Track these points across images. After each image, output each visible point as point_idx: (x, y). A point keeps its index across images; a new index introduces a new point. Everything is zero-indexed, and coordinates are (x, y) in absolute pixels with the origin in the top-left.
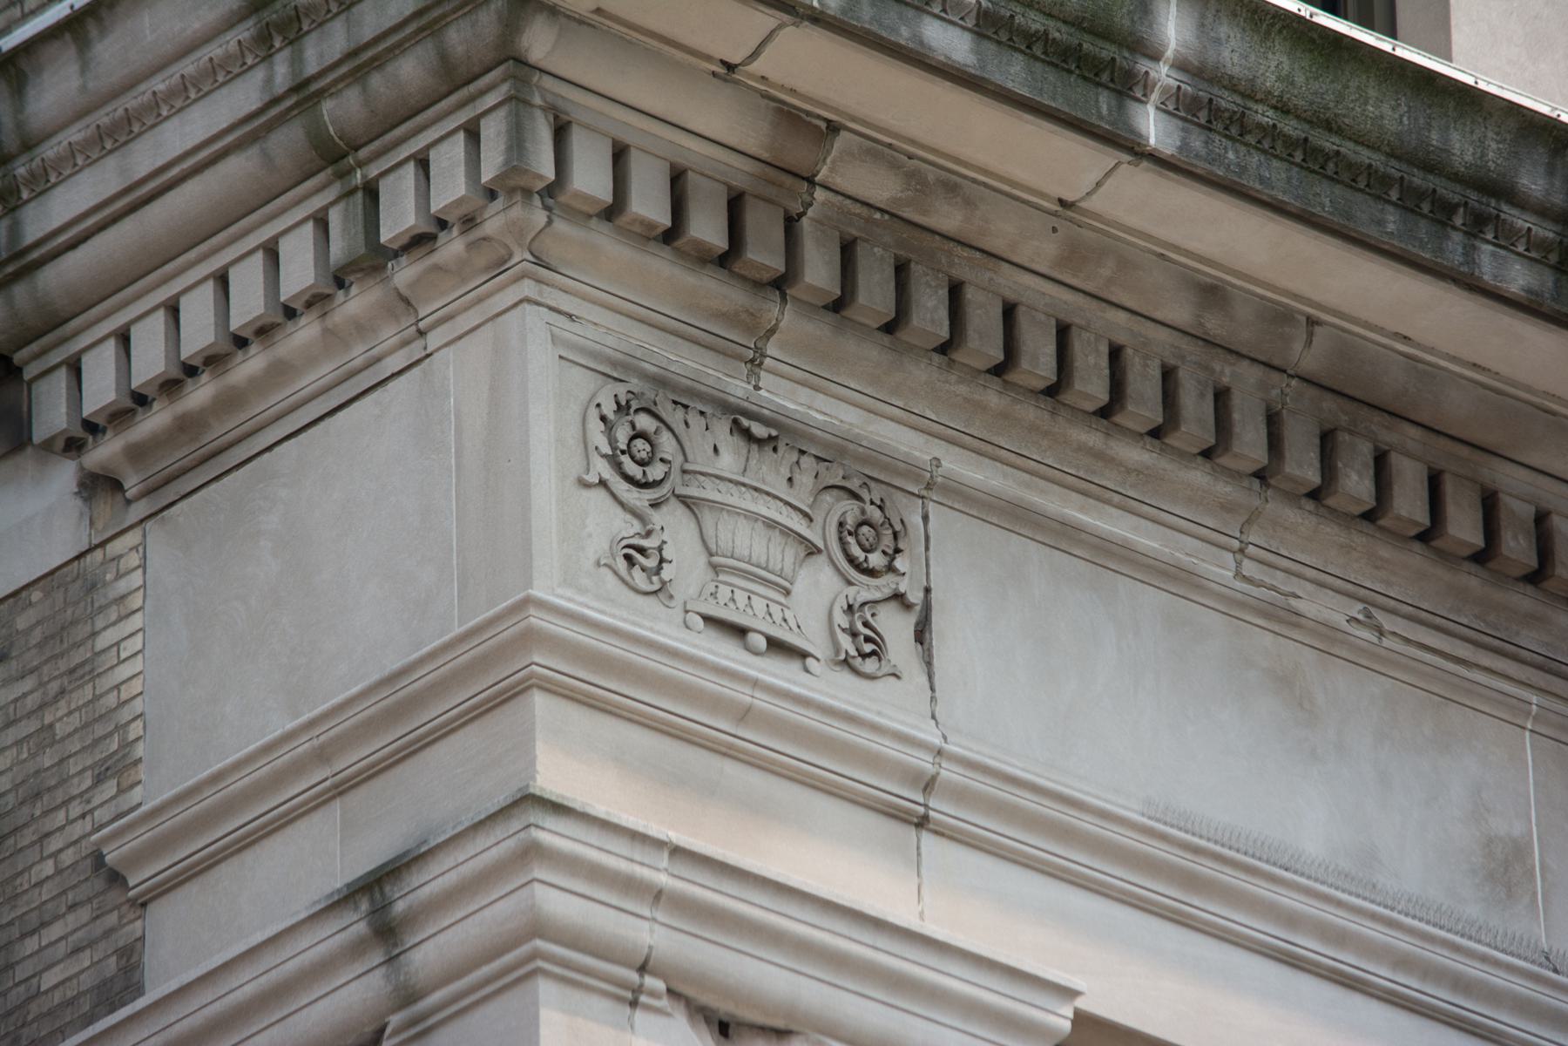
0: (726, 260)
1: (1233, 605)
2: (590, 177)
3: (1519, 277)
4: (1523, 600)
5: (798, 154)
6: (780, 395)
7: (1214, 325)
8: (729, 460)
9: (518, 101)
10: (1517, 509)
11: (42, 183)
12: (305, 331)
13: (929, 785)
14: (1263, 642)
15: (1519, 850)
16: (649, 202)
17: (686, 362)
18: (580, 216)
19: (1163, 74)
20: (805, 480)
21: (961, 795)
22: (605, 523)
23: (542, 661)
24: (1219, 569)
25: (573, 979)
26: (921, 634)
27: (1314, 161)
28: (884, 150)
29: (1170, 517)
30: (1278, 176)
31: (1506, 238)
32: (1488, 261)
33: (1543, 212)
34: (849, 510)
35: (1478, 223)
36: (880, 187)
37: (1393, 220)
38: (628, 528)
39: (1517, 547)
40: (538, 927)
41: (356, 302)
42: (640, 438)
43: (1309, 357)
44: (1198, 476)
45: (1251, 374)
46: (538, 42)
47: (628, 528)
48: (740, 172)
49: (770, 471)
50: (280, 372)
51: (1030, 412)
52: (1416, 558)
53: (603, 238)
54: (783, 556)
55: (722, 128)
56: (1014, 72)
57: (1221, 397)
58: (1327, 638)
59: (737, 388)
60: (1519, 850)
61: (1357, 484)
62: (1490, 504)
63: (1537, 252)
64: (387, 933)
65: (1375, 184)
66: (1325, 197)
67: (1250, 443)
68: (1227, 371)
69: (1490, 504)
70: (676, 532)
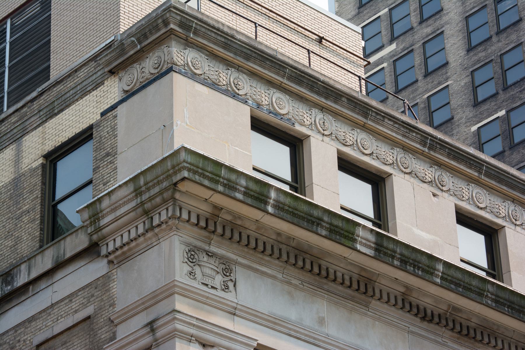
1: (282, 281)
3: (324, 233)
4: (325, 281)
5: (216, 213)
6: (213, 249)
7: (279, 239)
8: (205, 259)
9: (174, 204)
11: (103, 217)
12: (142, 239)
13: (235, 309)
14: (286, 287)
17: (199, 244)
19: (271, 201)
20: (217, 262)
21: (241, 310)
22: (187, 268)
23: (177, 289)
24: (280, 276)
25: (181, 338)
26: (235, 285)
27: (294, 215)
28: (230, 212)
30: (288, 217)
31: (322, 227)
32: (319, 230)
33: (327, 223)
35: (318, 224)
36: (229, 218)
37: (305, 224)
38: (190, 269)
40: (176, 330)
42: (192, 255)
44: (277, 262)
45: (285, 246)
46: (177, 196)
47: (190, 269)
50: (138, 245)
52: (309, 274)
53: (187, 225)
54: (213, 273)
55: (205, 209)
56: (249, 201)
58: (296, 287)
59: (207, 248)
60: (323, 318)
63: (327, 229)
65: (303, 218)
66: (296, 220)
68: (281, 246)
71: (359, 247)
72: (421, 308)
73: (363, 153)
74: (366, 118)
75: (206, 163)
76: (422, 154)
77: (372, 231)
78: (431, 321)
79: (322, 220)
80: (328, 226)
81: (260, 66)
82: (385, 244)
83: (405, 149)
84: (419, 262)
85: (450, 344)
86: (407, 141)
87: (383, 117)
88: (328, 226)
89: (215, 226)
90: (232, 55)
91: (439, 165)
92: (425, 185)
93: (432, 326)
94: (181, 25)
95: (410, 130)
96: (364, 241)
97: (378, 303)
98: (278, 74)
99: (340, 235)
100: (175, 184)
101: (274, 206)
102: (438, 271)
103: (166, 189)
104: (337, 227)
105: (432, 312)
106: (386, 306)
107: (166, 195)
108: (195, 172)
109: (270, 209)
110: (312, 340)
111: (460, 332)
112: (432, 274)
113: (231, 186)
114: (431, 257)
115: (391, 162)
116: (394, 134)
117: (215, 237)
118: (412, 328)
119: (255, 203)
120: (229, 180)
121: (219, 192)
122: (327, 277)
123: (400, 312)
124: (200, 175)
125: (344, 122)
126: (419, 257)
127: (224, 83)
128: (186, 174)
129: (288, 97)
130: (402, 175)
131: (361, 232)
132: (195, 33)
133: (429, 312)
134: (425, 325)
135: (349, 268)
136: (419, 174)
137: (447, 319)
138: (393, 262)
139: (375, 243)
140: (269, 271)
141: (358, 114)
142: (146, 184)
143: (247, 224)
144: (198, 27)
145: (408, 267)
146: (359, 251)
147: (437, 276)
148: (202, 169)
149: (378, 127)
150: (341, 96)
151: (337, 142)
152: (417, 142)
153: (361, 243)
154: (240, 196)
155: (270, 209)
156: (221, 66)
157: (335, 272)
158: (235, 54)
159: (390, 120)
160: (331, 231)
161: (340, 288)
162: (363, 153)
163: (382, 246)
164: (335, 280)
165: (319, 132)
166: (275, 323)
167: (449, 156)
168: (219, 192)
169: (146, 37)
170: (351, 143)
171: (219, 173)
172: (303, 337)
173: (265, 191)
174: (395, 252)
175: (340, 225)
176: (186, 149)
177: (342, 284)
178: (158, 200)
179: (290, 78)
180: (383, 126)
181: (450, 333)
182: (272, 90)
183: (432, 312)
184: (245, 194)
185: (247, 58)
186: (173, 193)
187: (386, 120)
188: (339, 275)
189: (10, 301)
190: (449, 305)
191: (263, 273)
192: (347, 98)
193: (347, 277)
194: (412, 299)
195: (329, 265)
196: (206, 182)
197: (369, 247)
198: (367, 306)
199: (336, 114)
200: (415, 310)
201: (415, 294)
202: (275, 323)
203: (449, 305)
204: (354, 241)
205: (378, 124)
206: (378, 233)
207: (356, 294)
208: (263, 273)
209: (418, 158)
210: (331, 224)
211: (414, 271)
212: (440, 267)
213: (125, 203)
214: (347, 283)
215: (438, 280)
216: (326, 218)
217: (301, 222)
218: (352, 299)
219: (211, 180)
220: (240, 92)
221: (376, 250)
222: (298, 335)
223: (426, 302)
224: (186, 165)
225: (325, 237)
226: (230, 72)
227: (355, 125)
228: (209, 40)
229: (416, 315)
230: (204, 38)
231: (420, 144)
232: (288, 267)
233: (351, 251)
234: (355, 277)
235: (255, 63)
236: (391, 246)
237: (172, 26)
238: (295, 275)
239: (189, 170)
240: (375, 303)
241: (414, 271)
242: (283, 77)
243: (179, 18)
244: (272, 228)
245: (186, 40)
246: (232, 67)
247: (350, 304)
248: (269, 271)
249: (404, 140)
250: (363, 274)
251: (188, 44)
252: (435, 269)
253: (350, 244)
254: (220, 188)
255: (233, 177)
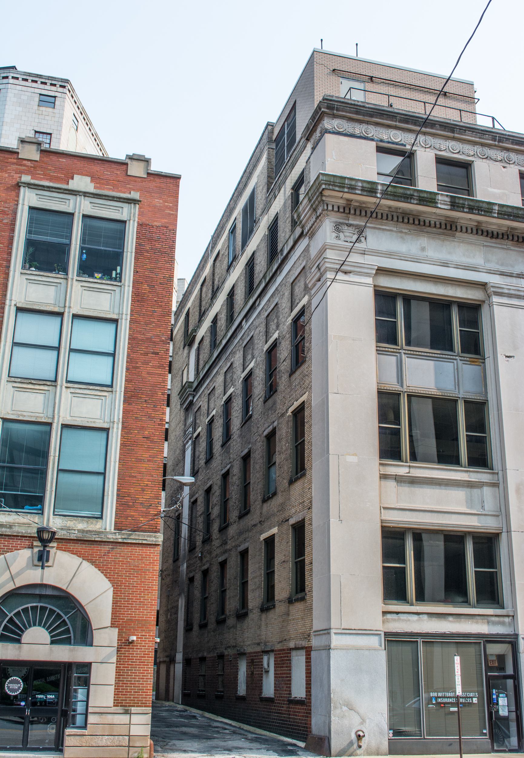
0: (344, 212)
1: (396, 232)
2: (330, 208)
3: (415, 202)
4: (423, 227)
5: (349, 203)
6: (351, 222)
7: (391, 210)
8: (346, 228)
9: (323, 203)
10: (422, 220)
11: (301, 215)
12: (316, 224)
13: (365, 251)
14: (399, 234)
15: (425, 247)
16: (336, 209)
17: (341, 221)
18: (330, 211)
19: (379, 191)
20: (354, 228)
21: (368, 251)
22: (334, 235)
23: (327, 247)
24: (395, 229)
25: (330, 271)
26: (366, 239)
27: (395, 196)
28: (357, 201)
29: (390, 226)
30: (391, 197)
31: (414, 199)
32: (412, 201)
33: (417, 196)
34: (358, 230)
35: (411, 198)
36: (357, 204)
37: (403, 199)
38: (336, 235)
39: (422, 223)
40: (326, 267)
41: (318, 221)
42: (338, 228)
43: (400, 211)
44: (391, 222)
45: (395, 213)
46: (324, 198)
47: (336, 235)
48: (344, 205)
49: (350, 228)
50: (315, 227)
51: (374, 220)
52: (413, 225)
53: (332, 213)
54: (351, 235)
55: (342, 202)
56: (365, 193)
57: (392, 216)
58: (406, 233)
59: (347, 222)
60: (425, 247)
61: (406, 220)
62: (419, 220)
63: (417, 200)
64: (319, 269)
65: (401, 197)
66: (396, 198)
67: (395, 219)
68: (398, 214)
69: (419, 220)
70: (341, 235)
71: (439, 206)
72: (490, 231)
73: (453, 153)
74: (453, 133)
75: (335, 178)
76: (495, 146)
77: (447, 196)
78: (497, 237)
79: (414, 196)
80: (417, 198)
81: (380, 119)
82: (457, 201)
83: (483, 145)
84: (481, 207)
85: (512, 248)
86: (483, 141)
87: (465, 130)
88: (417, 198)
89: (347, 209)
90: (361, 117)
91: (508, 150)
92: (497, 163)
93: (498, 241)
94: (328, 108)
95: (484, 134)
96: (442, 202)
97: (460, 233)
98: (392, 121)
99: (427, 201)
100: (321, 193)
101: (381, 193)
102: (495, 210)
103: (318, 196)
104: (423, 197)
105: (498, 233)
106: (466, 234)
107: (319, 199)
108: (329, 185)
109: (379, 195)
110: (415, 260)
111: (518, 241)
112: (491, 212)
113: (352, 188)
114: (489, 203)
115: (473, 154)
116: (473, 138)
117: (351, 216)
118: (485, 244)
119: (369, 194)
120: (350, 185)
121: (346, 192)
122: (424, 225)
123: (476, 236)
124: (333, 185)
125: (440, 138)
126: (481, 204)
127: (358, 132)
128: (324, 186)
129: (401, 132)
130: (481, 160)
131: (440, 197)
132: (337, 110)
133: (495, 233)
134: (494, 240)
135: (438, 218)
136: (492, 158)
137: (508, 235)
138: (463, 210)
139: (450, 202)
140: (387, 228)
141: (448, 132)
142: (311, 195)
143: (369, 206)
144: (339, 107)
145: (474, 211)
146: (440, 208)
147: (495, 213)
148: (333, 182)
149: (462, 136)
150: (435, 124)
151: (435, 150)
152: (490, 140)
153: (441, 203)
154: (359, 192)
155: (379, 195)
156: (357, 124)
157: (430, 222)
158: (364, 116)
159: (469, 131)
160: (420, 200)
161: (434, 229)
162: (453, 153)
163: (455, 203)
164: (430, 226)
165: (423, 147)
166: (391, 255)
167: (512, 143)
168: (346, 192)
169: (315, 118)
170: (444, 149)
171: (344, 182)
172: (410, 259)
173: (374, 186)
174: (464, 204)
175: (426, 196)
176: (322, 174)
177: (435, 227)
178: (317, 202)
179: (400, 121)
180: (465, 135)
181: (511, 242)
182: (390, 130)
183: (498, 233)
184: (362, 190)
185: (371, 116)
186: (321, 198)
187: (467, 132)
188: (432, 223)
189: (284, 263)
190: (508, 228)
191: (383, 229)
192: (440, 125)
193: (438, 223)
194: (483, 228)
195: (425, 218)
196: (337, 189)
197: (447, 205)
198: (454, 236)
199: (434, 135)
200: (485, 234)
201: (484, 225)
202: (391, 255)
203: (508, 228)
204: (437, 203)
205: (462, 135)
206: (451, 196)
207: (445, 231)
208: (383, 229)
209: (492, 148)
210: (419, 197)
211: (479, 212)
212: (496, 208)
213: (307, 207)
214: (438, 226)
215: (496, 215)
216: (416, 194)
217: (400, 199)
218: (443, 234)
219: (340, 187)
220: (369, 136)
221: (451, 205)
222: (406, 259)
223: (493, 228)
224: (323, 182)
225: (417, 204)
226: (362, 126)
227: (447, 138)
228: (346, 112)
229: (487, 236)
230: (343, 111)
231: (492, 140)
232: (399, 223)
233: (436, 209)
234: (443, 222)
235: (377, 118)
236: (461, 202)
237: (323, 109)
238: (404, 228)
239: (326, 184)
240: (458, 234)
241: (479, 212)
242: (396, 121)
243: (326, 104)
244: (385, 205)
245: (333, 115)
246: (363, 123)
247: (442, 237)
248: (387, 228)
249: (481, 140)
250: (448, 219)
251: (335, 116)
252: (493, 209)
253: (434, 205)
254: (346, 190)
255: (353, 183)
